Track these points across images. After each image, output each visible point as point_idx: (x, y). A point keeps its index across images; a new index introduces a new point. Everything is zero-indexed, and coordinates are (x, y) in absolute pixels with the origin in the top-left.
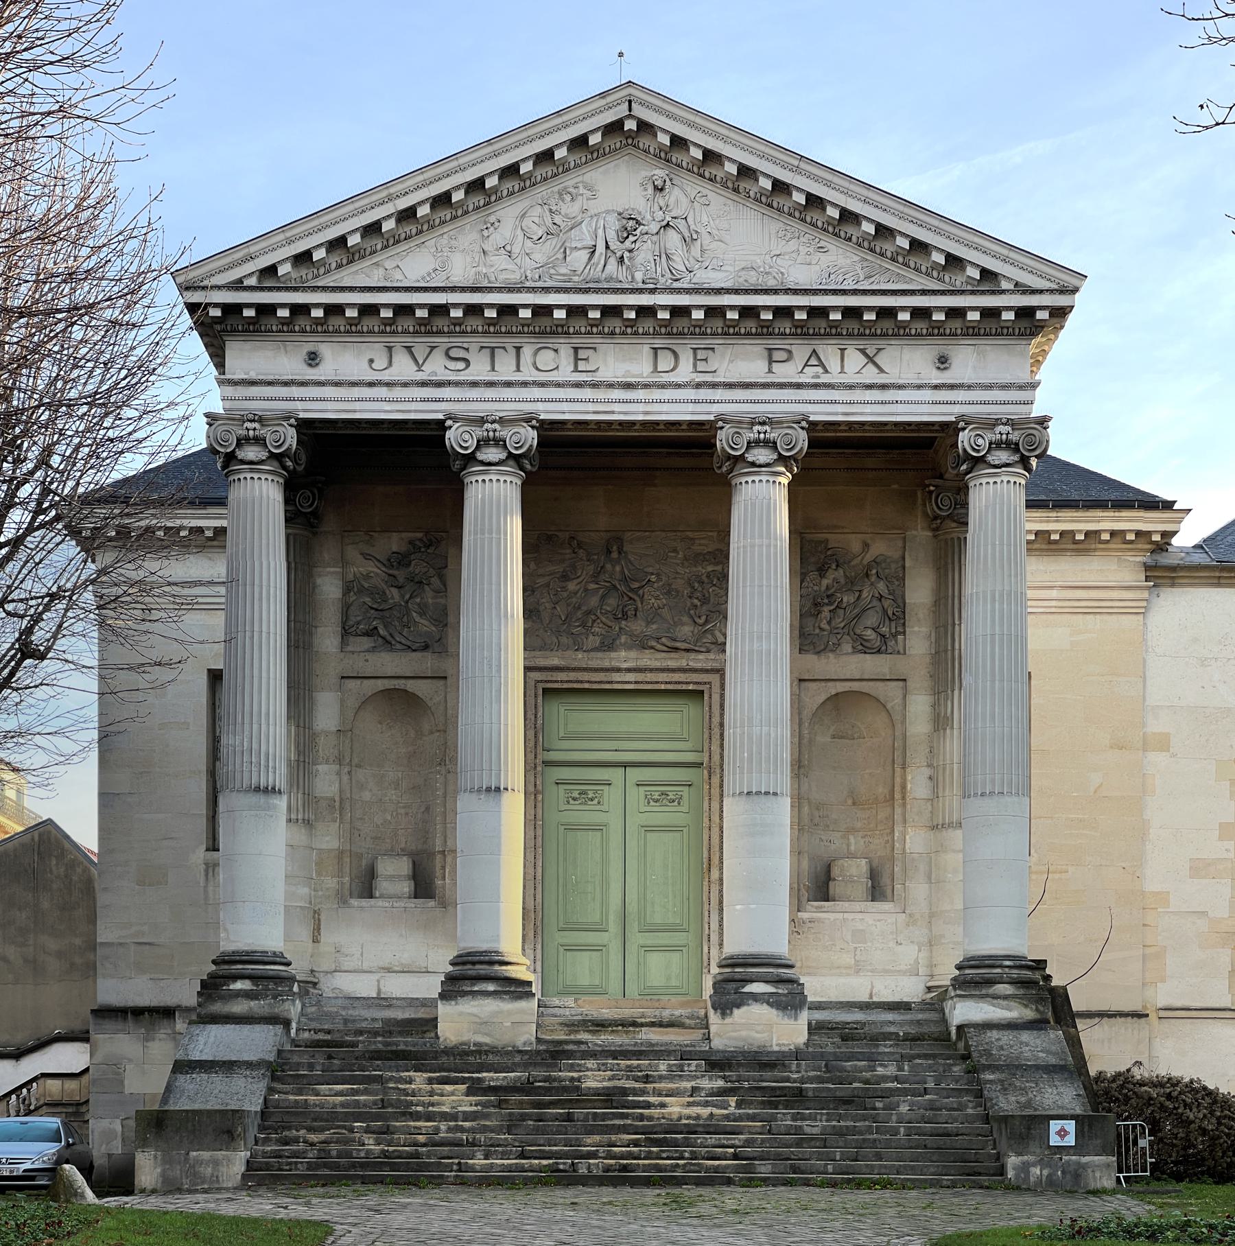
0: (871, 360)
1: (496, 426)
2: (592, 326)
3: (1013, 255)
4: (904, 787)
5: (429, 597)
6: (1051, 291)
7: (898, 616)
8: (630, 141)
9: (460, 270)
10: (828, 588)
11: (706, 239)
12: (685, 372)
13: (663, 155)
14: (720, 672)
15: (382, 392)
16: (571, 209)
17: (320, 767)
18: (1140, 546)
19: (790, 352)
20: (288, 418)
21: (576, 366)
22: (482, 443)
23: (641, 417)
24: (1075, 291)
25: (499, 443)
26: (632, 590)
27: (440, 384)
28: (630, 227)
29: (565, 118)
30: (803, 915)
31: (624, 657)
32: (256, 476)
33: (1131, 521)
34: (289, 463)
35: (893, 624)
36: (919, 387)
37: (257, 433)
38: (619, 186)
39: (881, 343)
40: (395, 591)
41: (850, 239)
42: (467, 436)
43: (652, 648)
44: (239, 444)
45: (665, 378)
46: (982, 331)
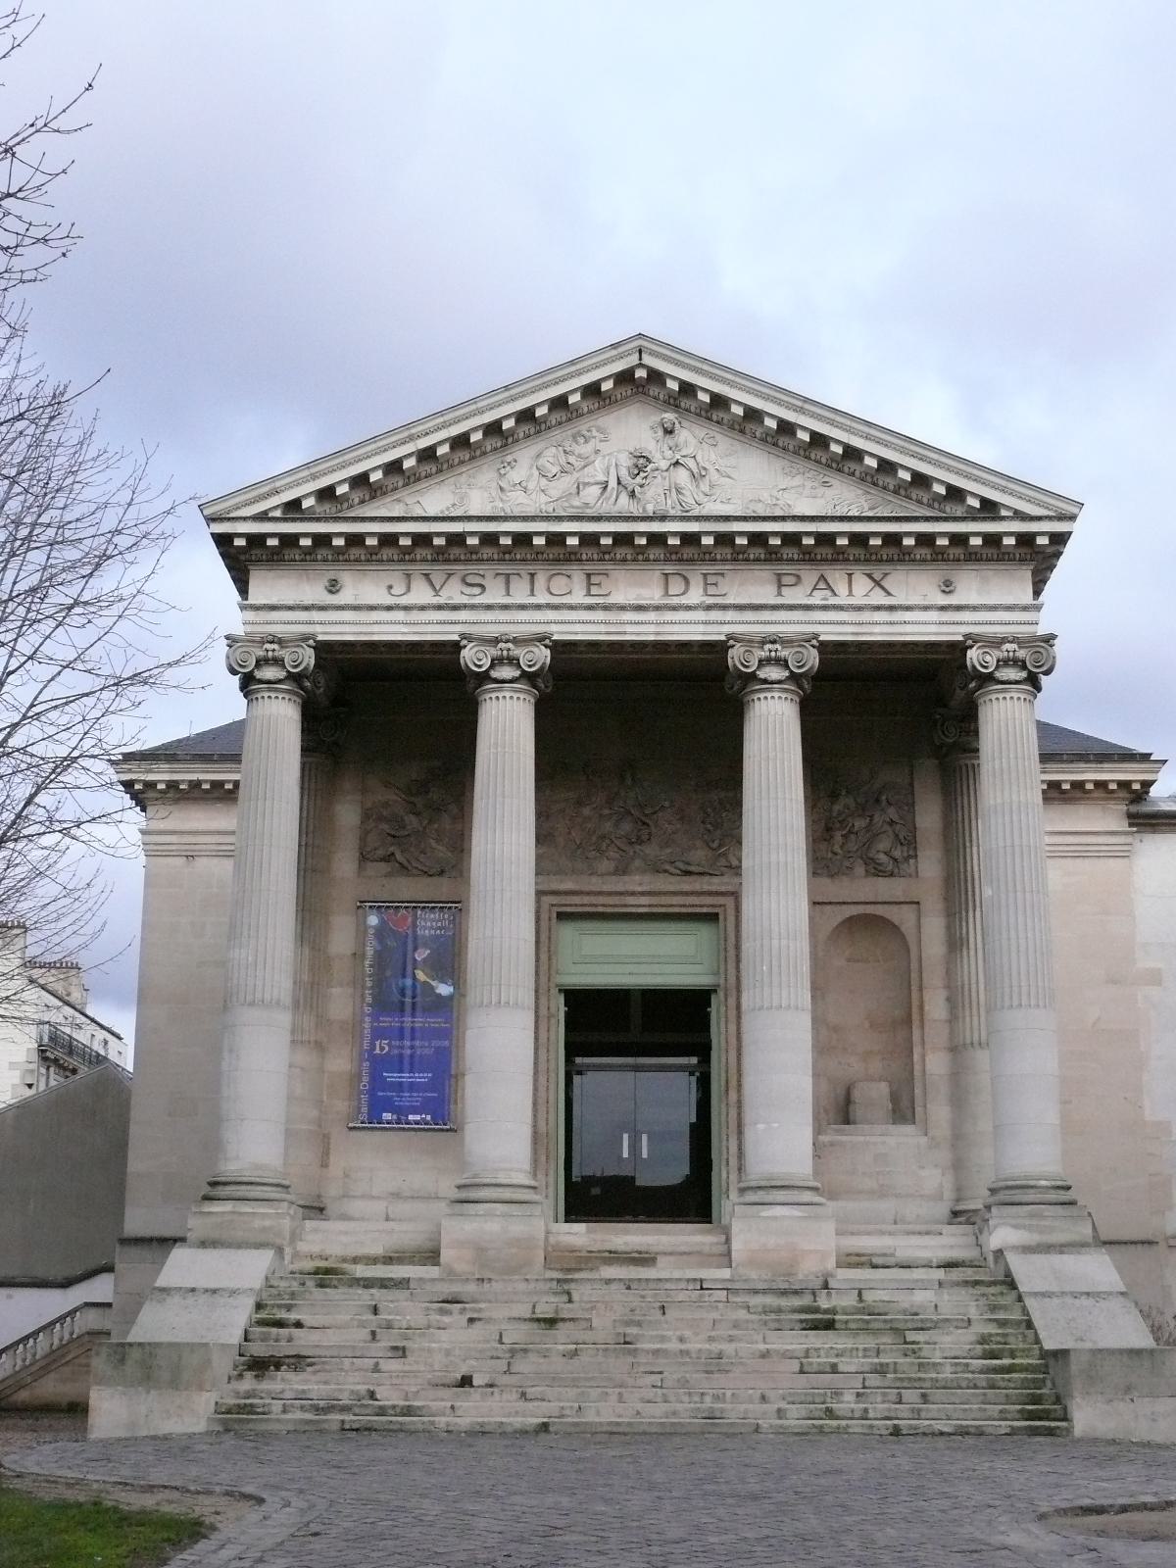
0: (878, 583)
1: (510, 645)
2: (604, 553)
3: (1011, 486)
4: (921, 1007)
5: (446, 822)
6: (1049, 518)
7: (910, 843)
8: (640, 390)
9: (478, 501)
10: (839, 814)
11: (714, 476)
12: (695, 596)
13: (672, 401)
14: (736, 895)
15: (400, 615)
16: (586, 449)
17: (334, 990)
18: (1121, 795)
19: (798, 577)
20: (308, 639)
21: (589, 590)
22: (497, 662)
23: (652, 638)
24: (1072, 518)
25: (513, 661)
26: (646, 815)
27: (455, 608)
28: (641, 464)
29: (578, 367)
30: (824, 1138)
31: (635, 882)
32: (273, 695)
33: (1112, 774)
34: (308, 684)
35: (905, 848)
36: (926, 608)
37: (276, 654)
38: (632, 430)
39: (887, 568)
40: (412, 818)
41: (853, 474)
42: (481, 655)
43: (666, 871)
44: (259, 664)
45: (675, 601)
46: (984, 556)
